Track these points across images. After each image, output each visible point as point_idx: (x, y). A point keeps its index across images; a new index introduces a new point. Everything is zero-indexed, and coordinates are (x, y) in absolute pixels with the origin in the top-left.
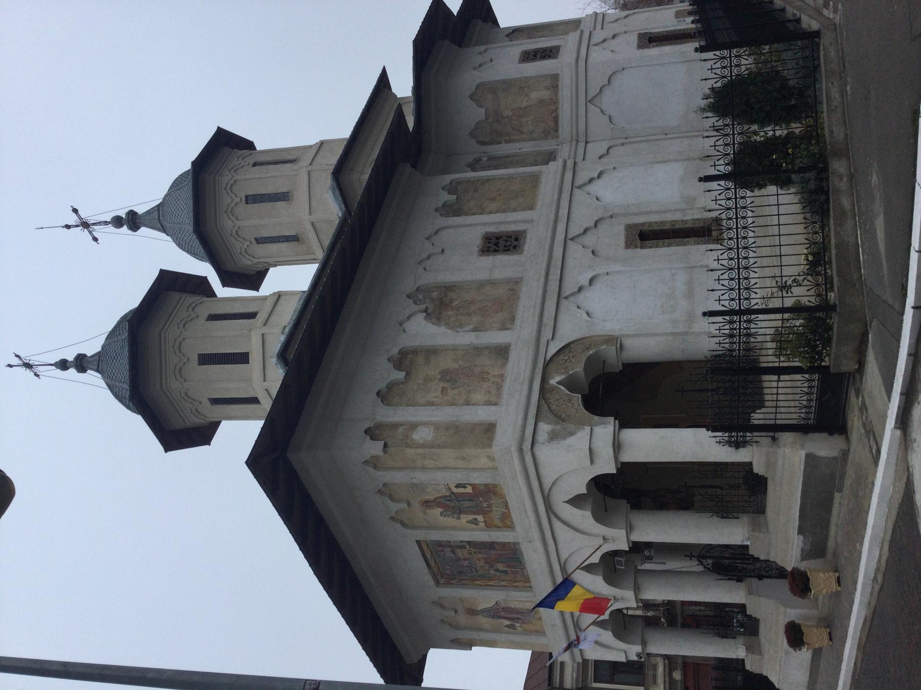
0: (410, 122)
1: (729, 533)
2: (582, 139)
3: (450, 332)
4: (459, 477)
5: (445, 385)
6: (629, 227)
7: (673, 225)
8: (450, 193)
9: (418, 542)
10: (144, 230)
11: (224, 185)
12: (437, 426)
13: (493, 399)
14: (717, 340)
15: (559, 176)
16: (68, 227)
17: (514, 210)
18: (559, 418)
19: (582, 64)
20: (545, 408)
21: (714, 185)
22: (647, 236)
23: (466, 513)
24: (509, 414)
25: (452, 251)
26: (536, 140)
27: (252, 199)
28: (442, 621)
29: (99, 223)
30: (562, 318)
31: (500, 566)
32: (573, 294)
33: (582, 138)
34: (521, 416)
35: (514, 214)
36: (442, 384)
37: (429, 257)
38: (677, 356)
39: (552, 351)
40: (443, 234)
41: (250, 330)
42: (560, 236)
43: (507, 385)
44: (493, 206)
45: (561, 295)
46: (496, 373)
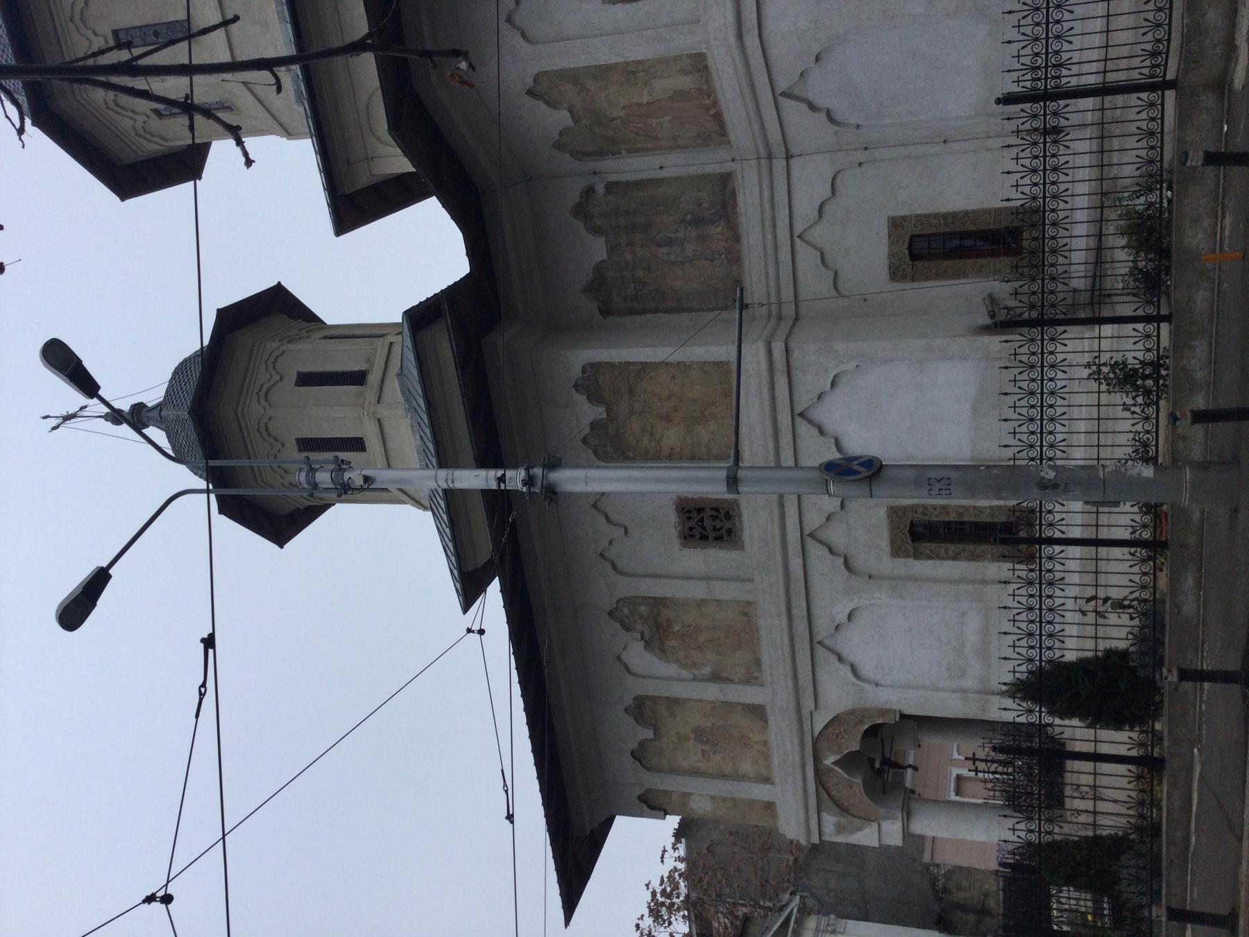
5: (705, 748)
7: (961, 514)
11: (68, 12)
14: (1015, 75)
15: (765, 382)
19: (752, 41)
21: (1014, 108)
27: (307, 379)
30: (823, 678)
33: (778, 150)
34: (801, 806)
36: (700, 747)
39: (818, 727)
42: (793, 536)
44: (672, 437)
45: (814, 644)
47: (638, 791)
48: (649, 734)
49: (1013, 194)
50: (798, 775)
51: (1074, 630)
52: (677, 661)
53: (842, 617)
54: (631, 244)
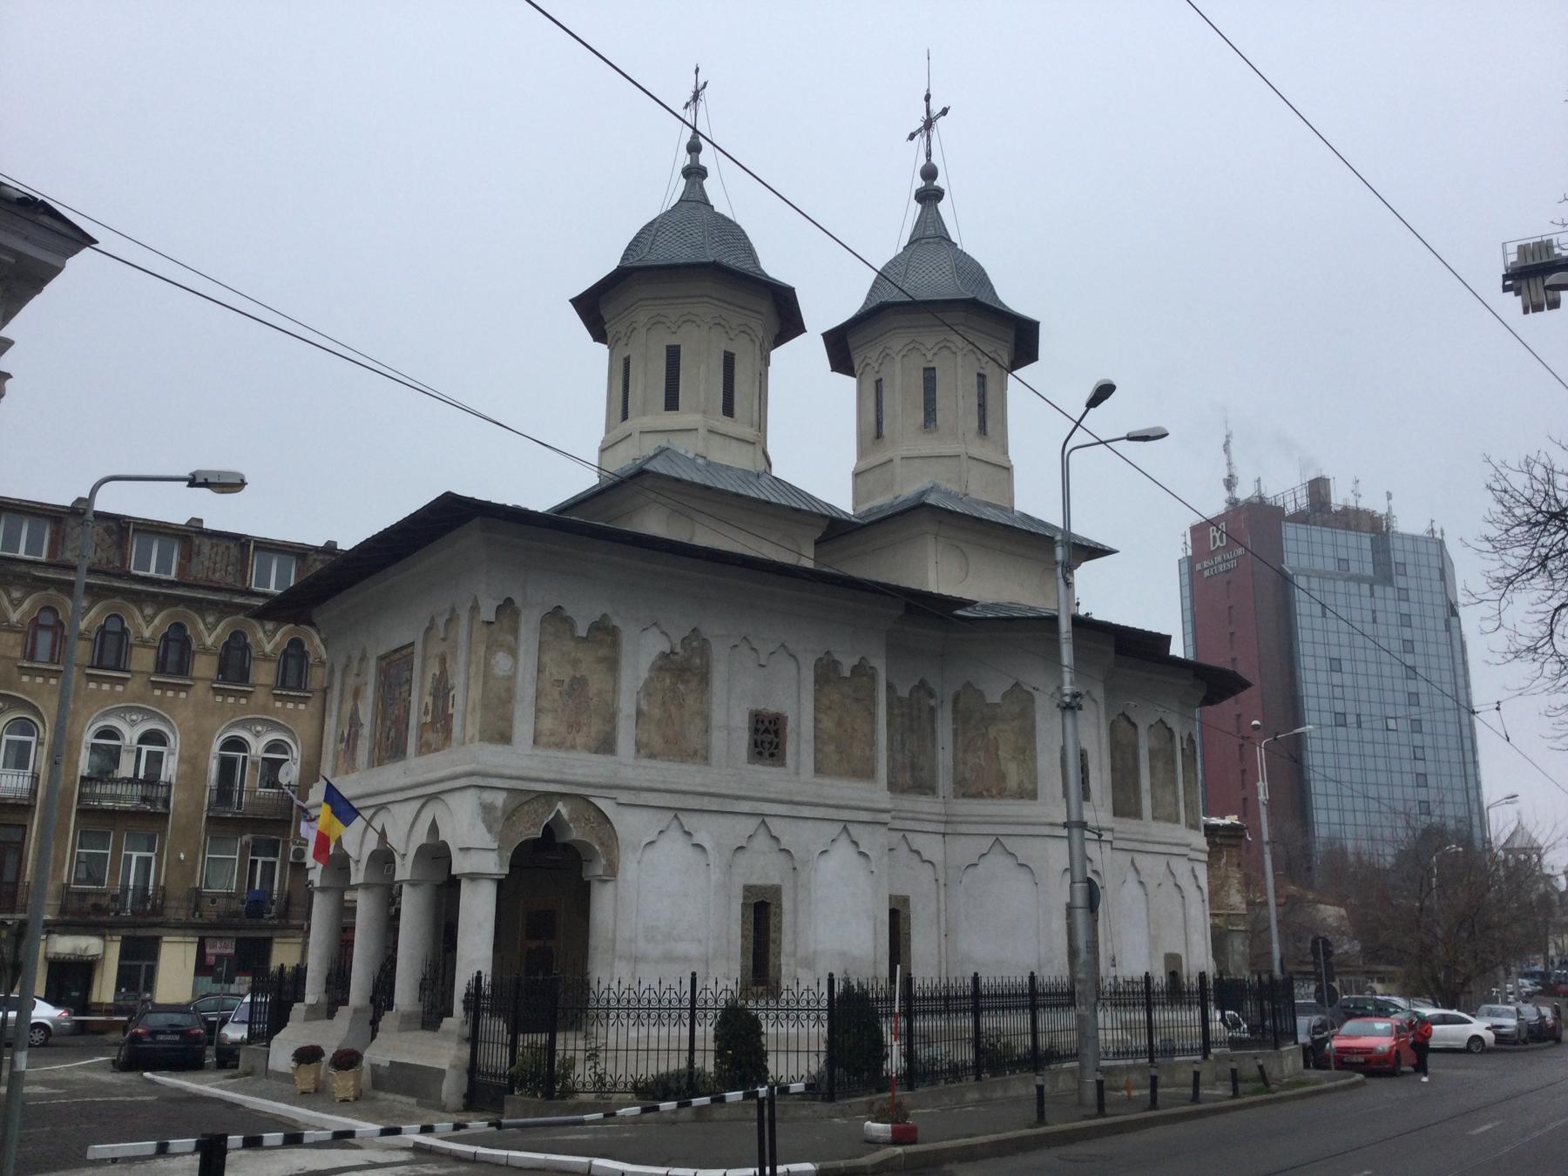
0: (959, 612)
1: (405, 993)
2: (948, 829)
3: (641, 684)
4: (459, 700)
5: (566, 686)
6: (776, 891)
8: (854, 670)
9: (412, 644)
10: (916, 208)
12: (511, 678)
13: (544, 739)
15: (867, 805)
16: (928, 98)
17: (817, 750)
18: (510, 815)
20: (525, 798)
21: (687, 986)
22: (761, 914)
23: (434, 703)
24: (526, 759)
25: (762, 672)
26: (955, 769)
27: (930, 376)
28: (349, 657)
29: (929, 144)
30: (645, 815)
31: (392, 734)
32: (681, 825)
33: (949, 829)
34: (514, 773)
35: (811, 750)
36: (567, 680)
37: (753, 649)
38: (593, 942)
39: (601, 804)
40: (792, 665)
41: (704, 412)
43: (561, 754)
44: (828, 724)
45: (680, 811)
46: (578, 741)
47: (518, 602)
48: (582, 631)
49: (604, 985)
50: (551, 776)
51: (803, 1031)
52: (651, 679)
53: (697, 839)
54: (903, 715)
